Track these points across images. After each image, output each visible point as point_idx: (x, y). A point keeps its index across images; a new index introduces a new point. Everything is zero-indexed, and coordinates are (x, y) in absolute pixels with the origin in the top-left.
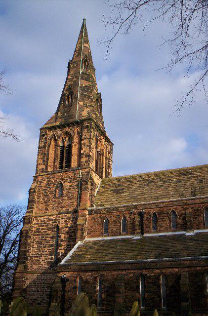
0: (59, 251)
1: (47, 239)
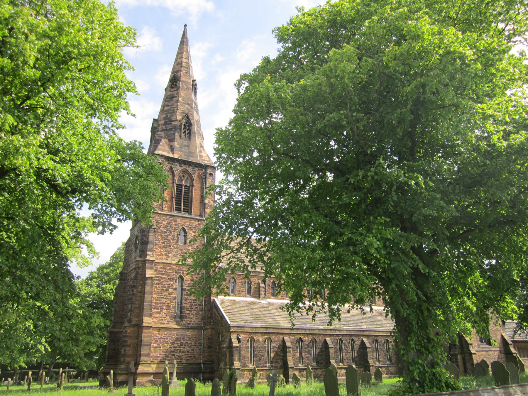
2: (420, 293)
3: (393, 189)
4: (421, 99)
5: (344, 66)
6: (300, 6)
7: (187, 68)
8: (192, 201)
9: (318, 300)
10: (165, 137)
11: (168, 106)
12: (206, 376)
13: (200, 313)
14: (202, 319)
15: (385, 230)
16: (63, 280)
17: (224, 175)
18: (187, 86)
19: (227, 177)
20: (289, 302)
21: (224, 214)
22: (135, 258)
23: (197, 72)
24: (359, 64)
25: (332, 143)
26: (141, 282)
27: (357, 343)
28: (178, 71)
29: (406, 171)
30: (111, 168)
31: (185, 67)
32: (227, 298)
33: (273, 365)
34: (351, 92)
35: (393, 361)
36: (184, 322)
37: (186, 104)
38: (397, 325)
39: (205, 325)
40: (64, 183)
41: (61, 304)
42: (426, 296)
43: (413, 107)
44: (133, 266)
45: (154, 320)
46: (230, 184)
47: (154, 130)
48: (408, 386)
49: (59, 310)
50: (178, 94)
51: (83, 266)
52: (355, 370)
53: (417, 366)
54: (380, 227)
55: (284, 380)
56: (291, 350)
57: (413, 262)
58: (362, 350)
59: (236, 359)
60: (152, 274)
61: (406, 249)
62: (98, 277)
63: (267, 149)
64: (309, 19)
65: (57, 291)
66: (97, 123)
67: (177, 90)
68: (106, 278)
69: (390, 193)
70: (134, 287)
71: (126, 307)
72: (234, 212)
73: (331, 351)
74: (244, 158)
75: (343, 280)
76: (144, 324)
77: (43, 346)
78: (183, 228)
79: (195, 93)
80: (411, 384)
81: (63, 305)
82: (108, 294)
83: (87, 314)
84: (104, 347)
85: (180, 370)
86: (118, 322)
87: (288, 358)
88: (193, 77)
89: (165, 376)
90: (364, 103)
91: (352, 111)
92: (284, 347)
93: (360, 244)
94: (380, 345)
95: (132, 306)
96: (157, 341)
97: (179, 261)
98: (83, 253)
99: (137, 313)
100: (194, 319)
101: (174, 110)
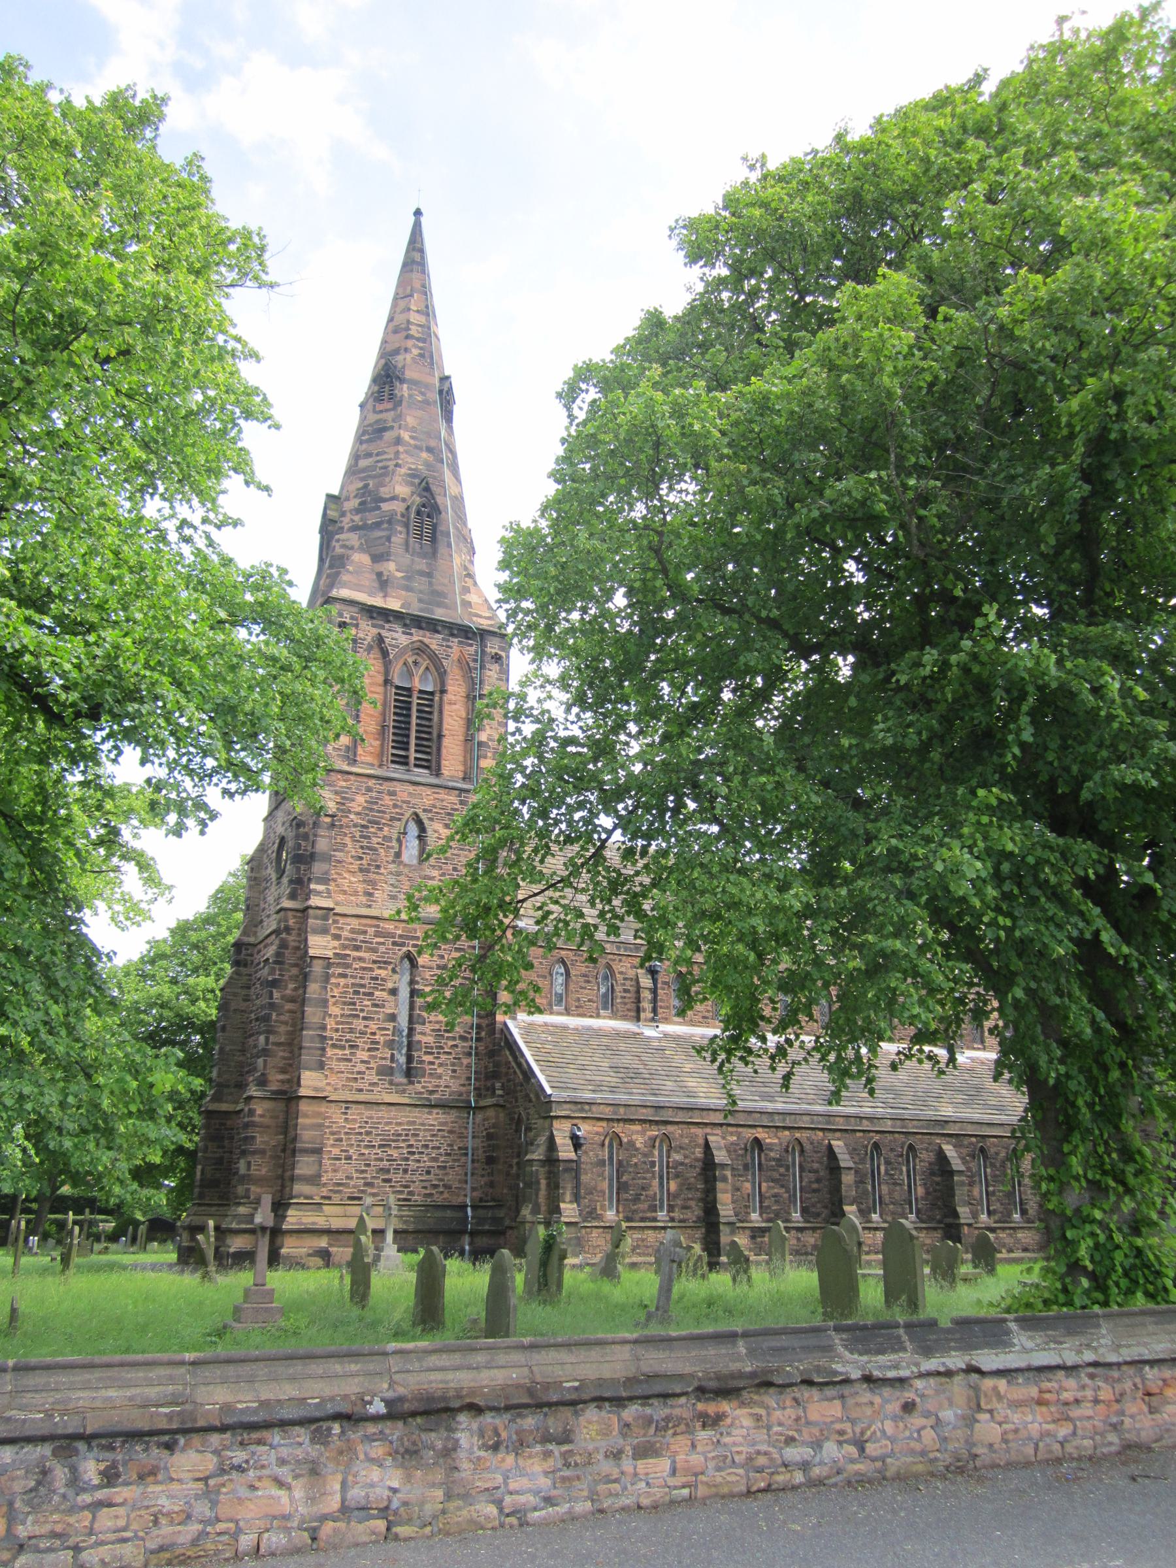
0: (417, 1037)
1: (377, 993)
2: (1100, 1015)
3: (1025, 708)
4: (1113, 436)
5: (881, 335)
6: (754, 155)
7: (424, 341)
8: (440, 736)
9: (801, 1028)
10: (361, 549)
11: (369, 455)
12: (483, 1241)
13: (465, 1061)
14: (469, 1079)
15: (1001, 827)
16: (70, 967)
17: (533, 661)
18: (423, 394)
19: (539, 668)
20: (718, 1032)
21: (528, 777)
22: (278, 900)
23: (456, 356)
24: (926, 327)
25: (851, 566)
26: (295, 971)
27: (926, 1157)
28: (396, 352)
29: (1066, 652)
30: (200, 645)
31: (418, 339)
32: (538, 1018)
33: (676, 1215)
34: (902, 413)
35: (1031, 1212)
36: (418, 1087)
37: (419, 448)
38: (1033, 1105)
39: (479, 1096)
40: (65, 688)
41: (63, 1033)
42: (1120, 1024)
43: (1089, 460)
44: (271, 925)
45: (333, 1079)
46: (549, 687)
47: (329, 529)
48: (1059, 1285)
49: (60, 1050)
50: (399, 417)
51: (128, 923)
52: (912, 1237)
53: (1088, 1228)
54: (985, 819)
55: (706, 1259)
56: (728, 1173)
57: (1081, 925)
58: (938, 1179)
59: (568, 1197)
60: (325, 948)
61: (1060, 885)
62: (174, 955)
63: (650, 584)
64: (774, 191)
65: (52, 997)
66: (159, 511)
67: (394, 409)
68: (195, 956)
69: (1015, 719)
70: (274, 984)
71: (251, 1041)
72: (559, 772)
73: (848, 1179)
74: (584, 610)
75: (873, 972)
76: (303, 1092)
77: (17, 1150)
78: (416, 814)
79: (448, 416)
80: (1068, 1280)
81: (69, 1034)
82: (202, 1004)
83: (138, 1058)
84: (191, 1155)
85: (405, 1222)
86: (231, 1083)
87: (719, 1195)
88: (441, 368)
89: (359, 1240)
90: (941, 445)
91: (902, 469)
92: (709, 1166)
93: (924, 868)
94: (993, 1165)
95: (267, 1039)
96: (341, 1140)
97: (399, 912)
98: (126, 888)
99: (284, 1058)
100: (447, 1079)
101: (386, 467)
